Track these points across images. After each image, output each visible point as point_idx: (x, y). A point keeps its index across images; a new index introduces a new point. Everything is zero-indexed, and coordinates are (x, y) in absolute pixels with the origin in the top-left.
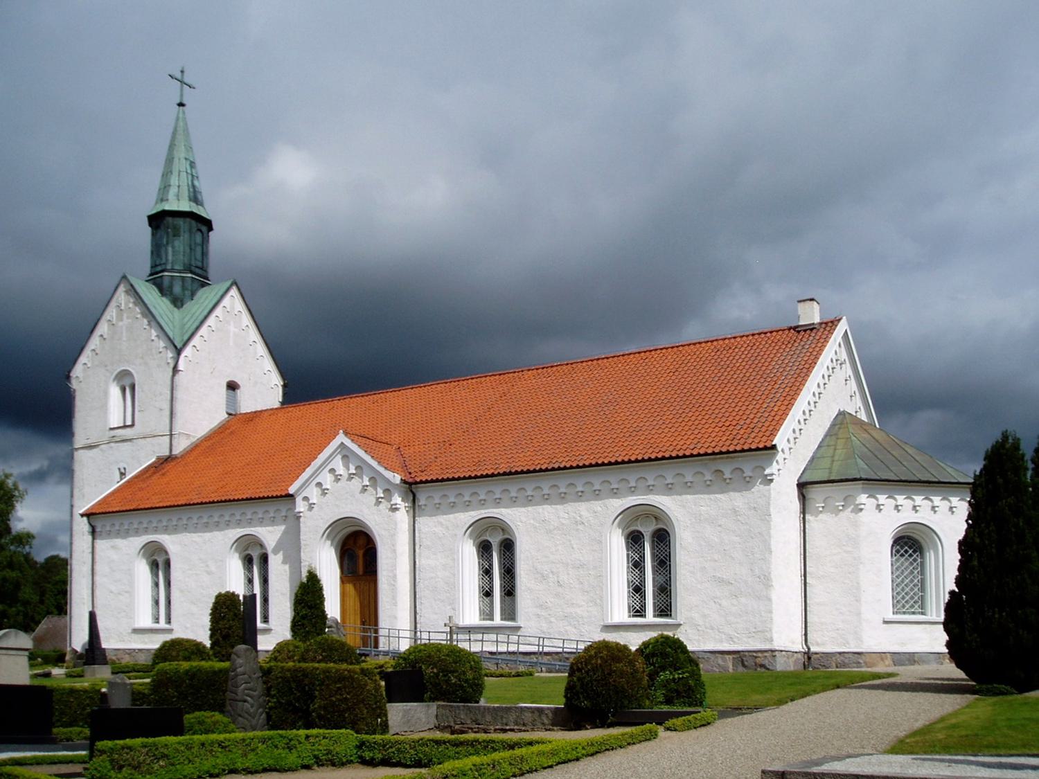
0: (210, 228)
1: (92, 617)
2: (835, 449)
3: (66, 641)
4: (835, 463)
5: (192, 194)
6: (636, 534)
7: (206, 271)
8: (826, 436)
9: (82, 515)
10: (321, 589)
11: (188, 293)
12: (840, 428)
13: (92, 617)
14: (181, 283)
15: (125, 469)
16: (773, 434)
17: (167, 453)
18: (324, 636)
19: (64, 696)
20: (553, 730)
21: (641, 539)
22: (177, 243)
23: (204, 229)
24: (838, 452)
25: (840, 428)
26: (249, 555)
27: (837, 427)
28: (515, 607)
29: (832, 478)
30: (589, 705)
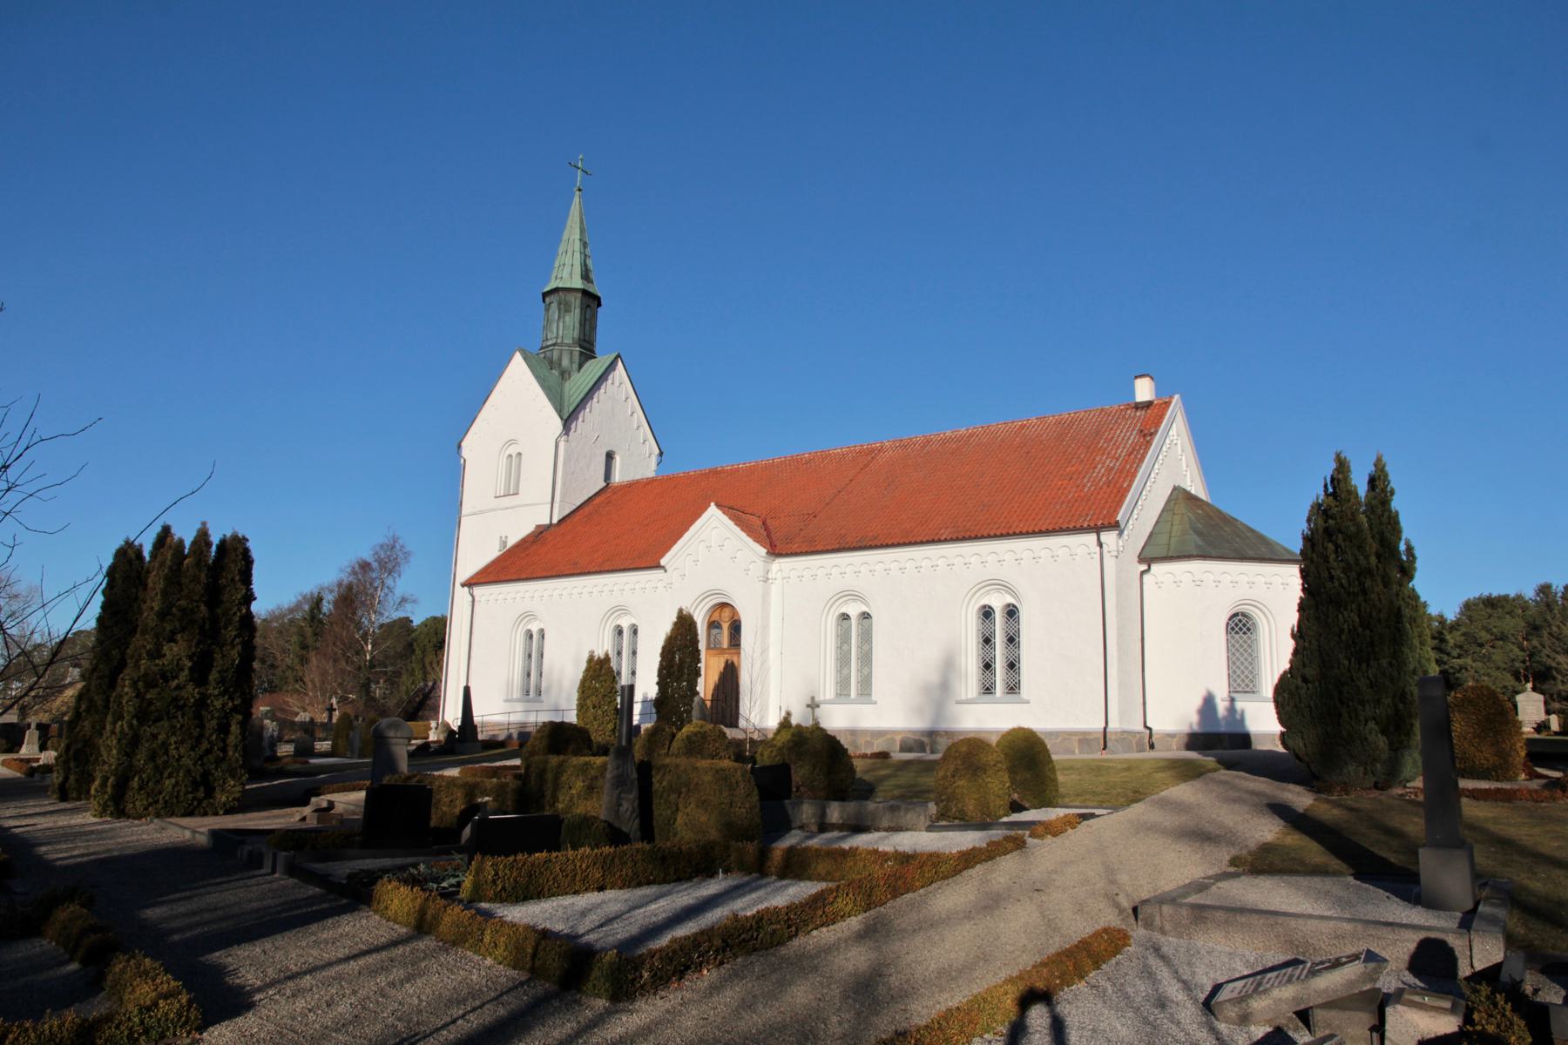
0: (599, 305)
1: (467, 692)
2: (1172, 525)
3: (439, 712)
4: (1172, 539)
5: (584, 273)
6: (1011, 608)
7: (593, 345)
8: (1163, 511)
9: (463, 585)
10: (664, 648)
11: (575, 366)
12: (1175, 504)
13: (467, 692)
14: (569, 356)
15: (506, 537)
16: (1116, 511)
17: (548, 522)
18: (1521, 930)
19: (323, 746)
20: (1204, 878)
21: (1015, 613)
22: (567, 318)
23: (594, 305)
24: (1175, 528)
25: (1175, 504)
26: (619, 626)
27: (1173, 502)
28: (1049, 732)
29: (1170, 555)
30: (1522, 932)
